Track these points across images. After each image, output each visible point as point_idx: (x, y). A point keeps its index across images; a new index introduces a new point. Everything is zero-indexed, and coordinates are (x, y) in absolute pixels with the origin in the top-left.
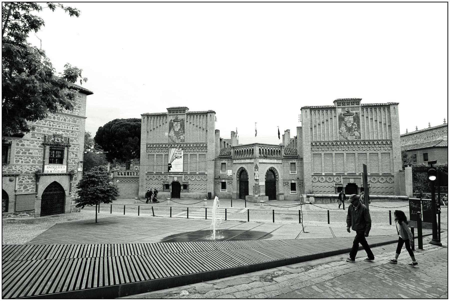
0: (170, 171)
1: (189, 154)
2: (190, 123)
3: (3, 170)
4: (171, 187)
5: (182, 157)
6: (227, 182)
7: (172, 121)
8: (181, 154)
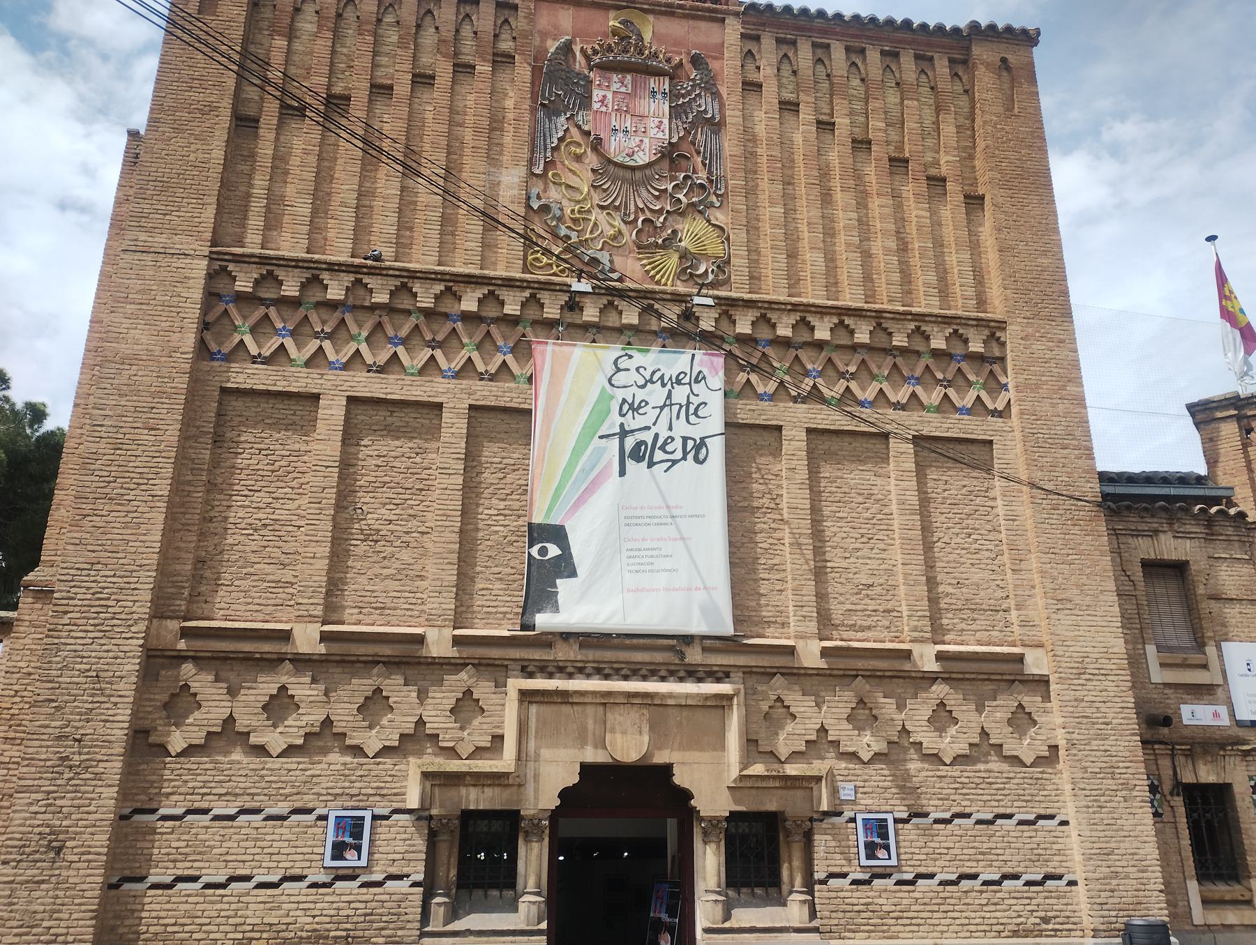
0: (543, 620)
1: (796, 419)
2: (789, 107)
3: (982, 53)
4: (533, 861)
5: (716, 448)
6: (1241, 789)
7: (580, 63)
8: (692, 411)
